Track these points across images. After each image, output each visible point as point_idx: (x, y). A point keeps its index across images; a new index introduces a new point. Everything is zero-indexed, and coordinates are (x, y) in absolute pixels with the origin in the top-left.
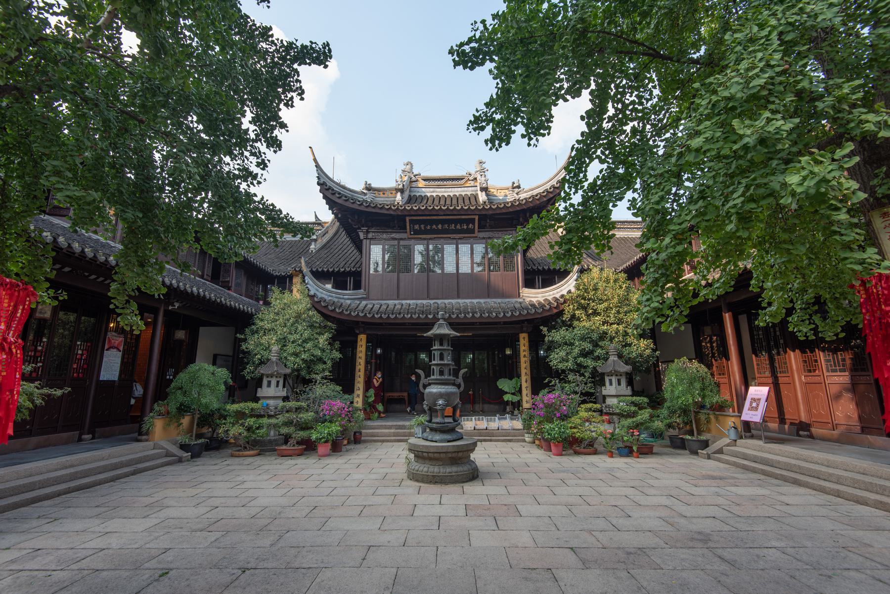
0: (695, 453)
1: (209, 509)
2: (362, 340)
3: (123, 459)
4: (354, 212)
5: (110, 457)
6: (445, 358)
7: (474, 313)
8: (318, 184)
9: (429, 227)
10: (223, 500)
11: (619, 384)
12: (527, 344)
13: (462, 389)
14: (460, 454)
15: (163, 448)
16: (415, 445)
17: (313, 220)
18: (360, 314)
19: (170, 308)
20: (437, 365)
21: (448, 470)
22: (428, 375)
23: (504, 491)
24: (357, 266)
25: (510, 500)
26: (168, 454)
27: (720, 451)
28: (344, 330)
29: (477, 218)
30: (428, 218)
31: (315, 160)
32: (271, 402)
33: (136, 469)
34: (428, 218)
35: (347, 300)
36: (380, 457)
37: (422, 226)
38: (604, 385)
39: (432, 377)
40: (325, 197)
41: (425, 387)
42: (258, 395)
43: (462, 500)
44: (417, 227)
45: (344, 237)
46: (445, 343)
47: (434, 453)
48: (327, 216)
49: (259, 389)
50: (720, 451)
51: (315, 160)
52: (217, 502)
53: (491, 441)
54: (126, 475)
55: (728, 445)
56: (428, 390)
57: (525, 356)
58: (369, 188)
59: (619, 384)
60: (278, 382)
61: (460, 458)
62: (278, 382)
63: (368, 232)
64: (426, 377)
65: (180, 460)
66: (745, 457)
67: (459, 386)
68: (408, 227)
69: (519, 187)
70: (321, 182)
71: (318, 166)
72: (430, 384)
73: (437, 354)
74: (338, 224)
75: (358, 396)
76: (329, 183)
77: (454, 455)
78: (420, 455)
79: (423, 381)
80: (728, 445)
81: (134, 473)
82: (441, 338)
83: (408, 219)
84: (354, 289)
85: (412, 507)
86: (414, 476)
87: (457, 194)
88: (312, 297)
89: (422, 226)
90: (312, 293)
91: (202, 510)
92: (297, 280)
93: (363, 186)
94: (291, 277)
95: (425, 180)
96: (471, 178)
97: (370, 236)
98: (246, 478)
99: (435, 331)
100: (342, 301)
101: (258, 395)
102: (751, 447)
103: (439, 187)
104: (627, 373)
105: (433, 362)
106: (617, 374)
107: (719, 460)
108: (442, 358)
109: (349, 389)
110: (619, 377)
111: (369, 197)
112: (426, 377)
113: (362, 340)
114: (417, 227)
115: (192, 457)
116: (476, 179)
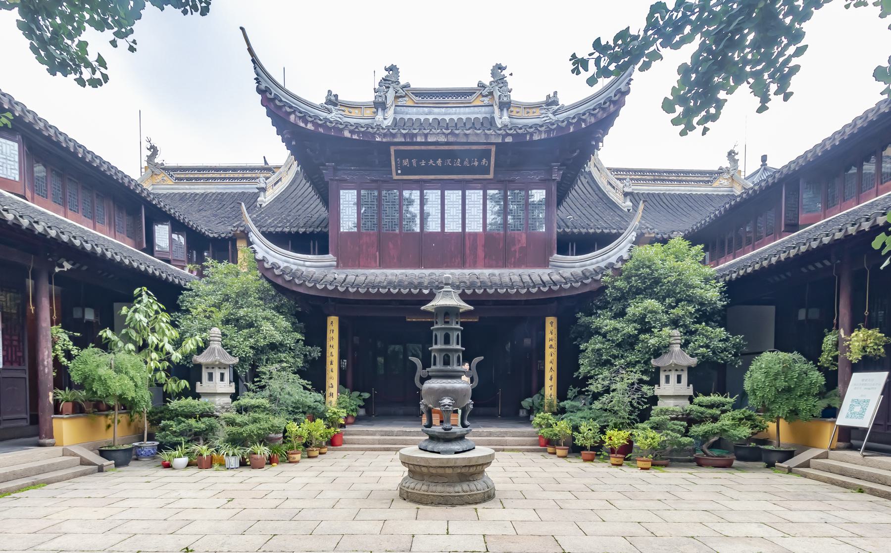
0: (770, 465)
1: (123, 537)
2: (333, 325)
3: (16, 468)
8: (259, 91)
10: (145, 524)
11: (679, 381)
12: (555, 332)
14: (472, 470)
15: (75, 455)
16: (409, 457)
17: (261, 163)
19: (57, 270)
20: (440, 350)
22: (426, 365)
23: (533, 516)
24: (323, 225)
25: (545, 529)
26: (84, 462)
27: (806, 465)
28: (308, 309)
29: (493, 149)
33: (37, 479)
35: (312, 268)
36: (362, 469)
37: (414, 161)
38: (659, 384)
41: (423, 380)
42: (197, 391)
43: (478, 529)
44: (406, 162)
45: (307, 188)
47: (435, 467)
48: (277, 151)
49: (198, 383)
50: (806, 465)
51: (250, 50)
52: (136, 527)
53: (503, 450)
54: (20, 489)
55: (817, 457)
56: (428, 385)
57: (551, 346)
58: (333, 101)
59: (679, 381)
60: (222, 375)
61: (472, 474)
62: (222, 375)
64: (424, 368)
65: (101, 469)
66: (843, 472)
68: (393, 163)
69: (555, 103)
70: (263, 87)
72: (429, 378)
73: (440, 336)
74: (295, 168)
75: (332, 395)
76: (275, 91)
77: (463, 470)
78: (416, 470)
79: (420, 372)
80: (817, 457)
81: (34, 485)
83: (392, 149)
84: (319, 254)
85: (409, 538)
86: (406, 496)
87: (464, 117)
88: (261, 262)
90: (259, 256)
91: (113, 538)
92: (241, 245)
93: (324, 101)
94: (233, 240)
95: (416, 95)
96: (485, 92)
98: (183, 494)
99: (440, 301)
100: (303, 269)
101: (197, 391)
102: (853, 460)
103: (438, 105)
104: (690, 369)
105: (435, 347)
107: (805, 476)
108: (447, 340)
109: (320, 386)
110: (679, 373)
111: (334, 115)
112: (424, 368)
113: (333, 325)
114: (406, 162)
115: (117, 465)
116: (491, 93)
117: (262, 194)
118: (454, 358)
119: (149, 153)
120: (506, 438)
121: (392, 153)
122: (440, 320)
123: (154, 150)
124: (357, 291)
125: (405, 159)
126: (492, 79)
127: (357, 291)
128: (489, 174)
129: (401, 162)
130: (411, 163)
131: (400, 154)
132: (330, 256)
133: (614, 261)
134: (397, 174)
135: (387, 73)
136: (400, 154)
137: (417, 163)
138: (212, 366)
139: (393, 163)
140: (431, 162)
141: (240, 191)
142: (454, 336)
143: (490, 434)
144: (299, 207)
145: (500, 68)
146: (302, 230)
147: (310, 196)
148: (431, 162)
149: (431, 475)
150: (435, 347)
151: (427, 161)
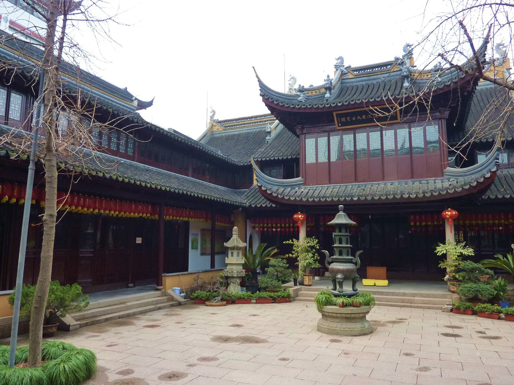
4: (290, 114)
5: (243, 130)
6: (343, 242)
7: (424, 193)
9: (354, 119)
13: (358, 266)
18: (310, 200)
21: (344, 326)
30: (352, 110)
31: (257, 76)
32: (234, 267)
34: (352, 110)
37: (348, 118)
39: (334, 257)
40: (267, 105)
41: (330, 263)
42: (226, 262)
44: (343, 119)
46: (343, 230)
51: (257, 76)
63: (303, 128)
67: (356, 264)
68: (336, 121)
71: (259, 81)
72: (333, 262)
79: (328, 259)
82: (340, 226)
86: (319, 329)
89: (348, 118)
97: (305, 131)
101: (226, 262)
105: (335, 245)
106: (238, 248)
117: (268, 135)
118: (344, 251)
119: (211, 114)
120: (416, 298)
121: (335, 115)
122: (337, 230)
123: (214, 112)
124: (314, 200)
125: (343, 117)
126: (404, 53)
127: (314, 200)
128: (397, 119)
129: (341, 120)
130: (346, 119)
131: (339, 116)
132: (300, 178)
133: (485, 173)
134: (339, 126)
135: (337, 61)
136: (339, 116)
137: (350, 119)
138: (233, 248)
139: (336, 121)
140: (359, 117)
141: (258, 130)
142: (344, 239)
143: (404, 294)
144: (290, 140)
145: (408, 46)
146: (289, 157)
147: (259, 197)
148: (359, 117)
149: (329, 317)
150: (335, 245)
151: (356, 117)
